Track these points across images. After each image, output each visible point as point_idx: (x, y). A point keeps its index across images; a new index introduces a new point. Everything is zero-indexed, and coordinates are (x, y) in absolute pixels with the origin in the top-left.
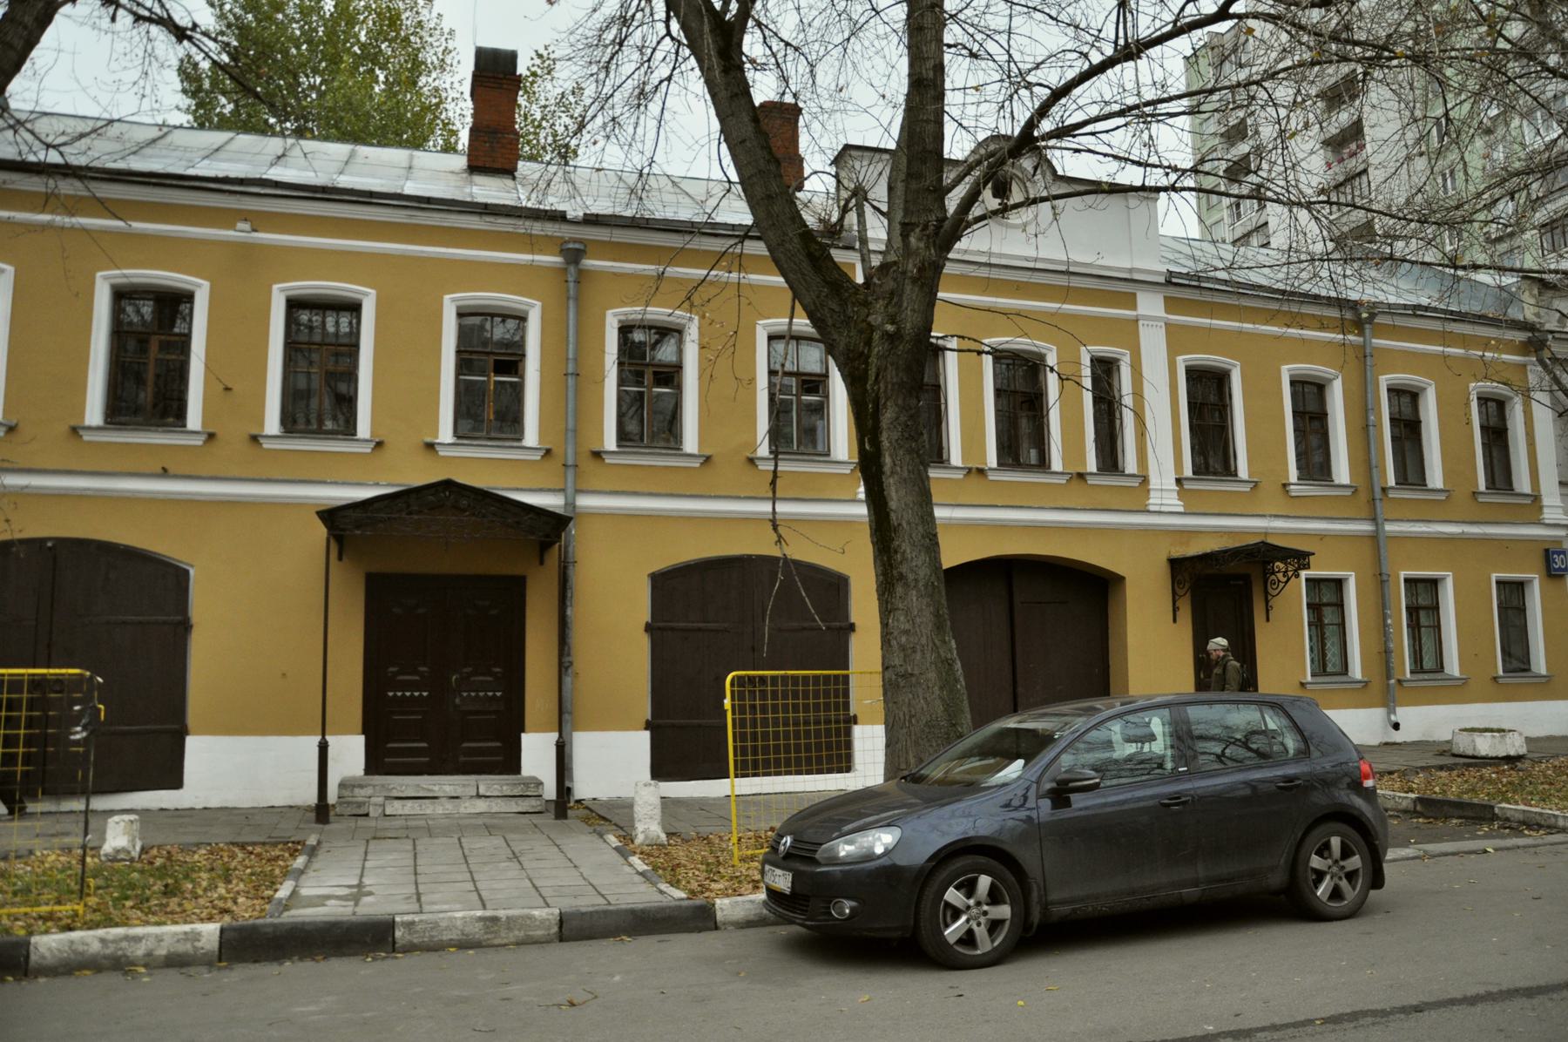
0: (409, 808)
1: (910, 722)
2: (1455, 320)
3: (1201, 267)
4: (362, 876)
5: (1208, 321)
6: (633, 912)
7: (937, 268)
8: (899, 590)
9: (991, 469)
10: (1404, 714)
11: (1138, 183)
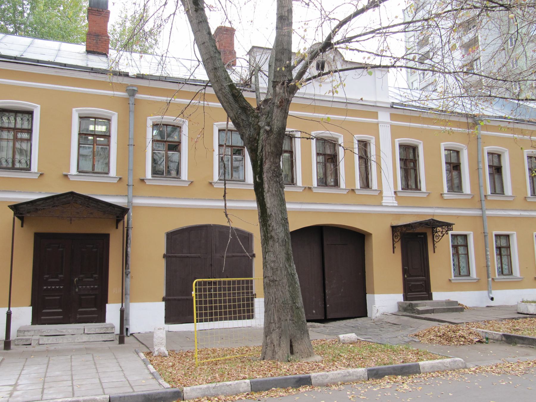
0: (51, 340)
1: (275, 301)
2: (517, 123)
3: (404, 100)
4: (18, 379)
5: (409, 124)
6: (144, 396)
7: (288, 102)
8: (271, 242)
9: (314, 187)
10: (495, 293)
11: (378, 64)
